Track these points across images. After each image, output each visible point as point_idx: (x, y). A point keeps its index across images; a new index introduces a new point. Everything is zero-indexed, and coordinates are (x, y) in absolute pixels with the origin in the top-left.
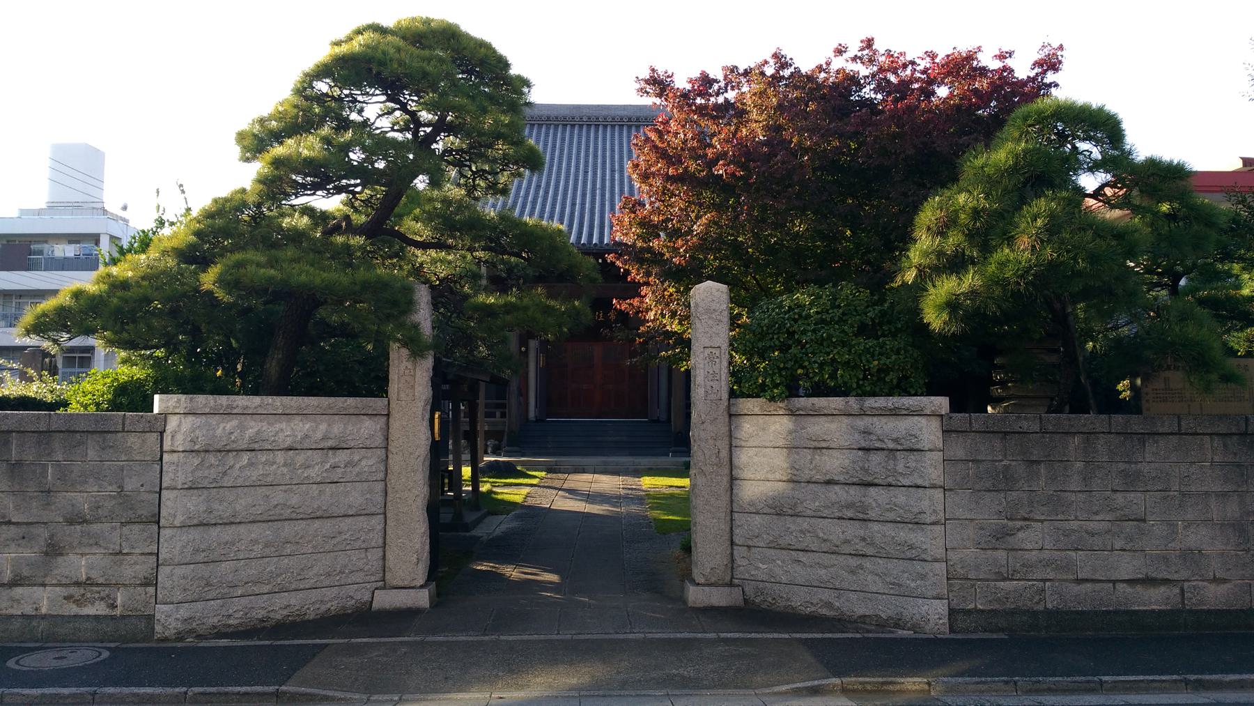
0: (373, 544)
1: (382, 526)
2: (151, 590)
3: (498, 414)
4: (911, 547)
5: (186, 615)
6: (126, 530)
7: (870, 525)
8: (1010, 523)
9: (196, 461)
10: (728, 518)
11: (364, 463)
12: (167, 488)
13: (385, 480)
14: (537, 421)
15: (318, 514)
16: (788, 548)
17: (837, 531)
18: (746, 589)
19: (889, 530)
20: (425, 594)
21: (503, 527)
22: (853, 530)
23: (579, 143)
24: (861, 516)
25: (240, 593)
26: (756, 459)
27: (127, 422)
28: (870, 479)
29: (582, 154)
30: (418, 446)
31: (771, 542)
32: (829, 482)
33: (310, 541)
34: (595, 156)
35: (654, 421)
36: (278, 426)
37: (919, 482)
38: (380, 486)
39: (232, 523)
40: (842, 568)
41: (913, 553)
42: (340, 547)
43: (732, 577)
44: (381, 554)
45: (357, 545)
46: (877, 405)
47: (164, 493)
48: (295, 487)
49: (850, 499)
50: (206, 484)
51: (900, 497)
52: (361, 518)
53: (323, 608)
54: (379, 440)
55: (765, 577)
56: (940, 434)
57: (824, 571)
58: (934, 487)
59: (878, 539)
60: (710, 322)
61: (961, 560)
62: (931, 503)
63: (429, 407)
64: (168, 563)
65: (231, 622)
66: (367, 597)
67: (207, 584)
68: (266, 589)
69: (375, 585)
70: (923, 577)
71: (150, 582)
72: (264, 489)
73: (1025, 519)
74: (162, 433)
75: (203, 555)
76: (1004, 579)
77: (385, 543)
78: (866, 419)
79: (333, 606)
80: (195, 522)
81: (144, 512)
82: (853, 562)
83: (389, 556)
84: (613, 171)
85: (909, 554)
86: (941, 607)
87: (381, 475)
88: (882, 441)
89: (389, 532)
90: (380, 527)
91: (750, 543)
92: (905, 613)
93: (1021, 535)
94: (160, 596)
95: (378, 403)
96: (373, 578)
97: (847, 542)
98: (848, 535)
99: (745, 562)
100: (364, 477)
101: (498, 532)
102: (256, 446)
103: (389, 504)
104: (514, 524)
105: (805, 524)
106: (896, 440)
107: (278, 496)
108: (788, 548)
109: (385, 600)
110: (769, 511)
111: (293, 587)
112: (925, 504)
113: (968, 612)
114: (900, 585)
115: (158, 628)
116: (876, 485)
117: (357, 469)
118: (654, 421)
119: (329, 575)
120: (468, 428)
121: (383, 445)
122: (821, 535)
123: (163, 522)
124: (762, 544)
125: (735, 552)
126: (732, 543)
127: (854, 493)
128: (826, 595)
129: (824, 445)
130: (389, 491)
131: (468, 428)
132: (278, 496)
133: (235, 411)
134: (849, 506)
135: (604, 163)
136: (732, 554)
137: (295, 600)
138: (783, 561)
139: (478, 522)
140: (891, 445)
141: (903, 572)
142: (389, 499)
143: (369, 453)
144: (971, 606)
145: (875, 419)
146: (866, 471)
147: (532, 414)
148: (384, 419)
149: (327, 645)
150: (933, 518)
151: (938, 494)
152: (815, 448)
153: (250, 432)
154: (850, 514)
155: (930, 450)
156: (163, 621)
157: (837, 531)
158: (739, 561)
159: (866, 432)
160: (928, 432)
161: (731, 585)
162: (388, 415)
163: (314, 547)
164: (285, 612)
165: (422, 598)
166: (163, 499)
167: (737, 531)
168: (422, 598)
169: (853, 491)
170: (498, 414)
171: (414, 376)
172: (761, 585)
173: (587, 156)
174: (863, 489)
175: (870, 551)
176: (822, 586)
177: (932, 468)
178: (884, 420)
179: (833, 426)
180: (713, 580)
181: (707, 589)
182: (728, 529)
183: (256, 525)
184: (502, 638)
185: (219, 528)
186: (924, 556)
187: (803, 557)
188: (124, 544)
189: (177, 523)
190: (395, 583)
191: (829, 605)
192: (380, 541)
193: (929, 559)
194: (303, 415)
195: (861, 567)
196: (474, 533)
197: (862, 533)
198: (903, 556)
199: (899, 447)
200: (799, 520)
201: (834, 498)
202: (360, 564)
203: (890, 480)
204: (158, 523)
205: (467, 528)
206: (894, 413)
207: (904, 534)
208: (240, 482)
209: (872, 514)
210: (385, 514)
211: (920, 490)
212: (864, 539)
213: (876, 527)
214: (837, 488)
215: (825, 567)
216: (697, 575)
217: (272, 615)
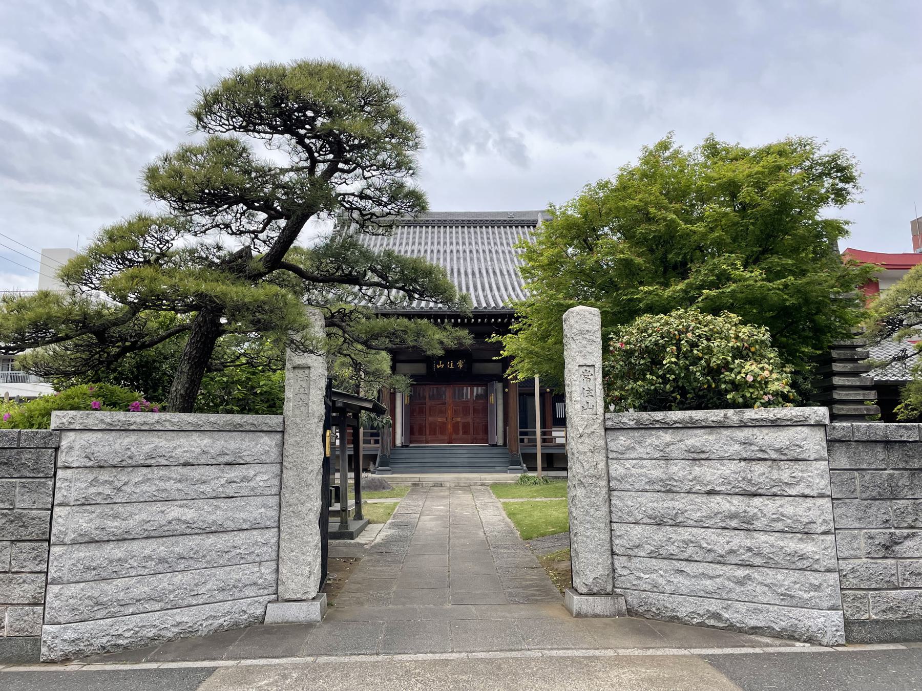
0: (267, 558)
1: (276, 539)
2: (39, 609)
3: (372, 442)
4: (802, 557)
5: (74, 636)
6: (15, 549)
7: (755, 534)
8: (897, 531)
9: (91, 477)
10: (608, 529)
11: (258, 478)
12: (60, 505)
13: (279, 494)
14: (402, 446)
15: (213, 528)
16: (670, 557)
17: (720, 541)
18: (629, 599)
19: (771, 538)
20: (317, 605)
21: (383, 534)
22: (739, 540)
23: (432, 239)
24: (746, 526)
25: (131, 611)
26: (634, 471)
27: (23, 438)
28: (754, 489)
29: (435, 246)
30: (312, 462)
31: (652, 552)
32: (710, 493)
33: (204, 556)
34: (445, 248)
35: (493, 446)
36: (176, 443)
37: (807, 492)
38: (273, 501)
39: (125, 539)
40: (729, 579)
41: (806, 563)
42: (234, 561)
43: (614, 587)
44: (275, 567)
45: (250, 559)
46: (756, 417)
47: (56, 509)
48: (191, 503)
49: (733, 509)
50: (99, 500)
51: (789, 508)
52: (255, 532)
53: (217, 623)
54: (274, 454)
55: (648, 587)
56: (824, 444)
57: (708, 582)
58: (822, 496)
59: (766, 550)
60: (584, 342)
61: (853, 570)
62: (819, 512)
63: (322, 424)
64: (55, 582)
65: (121, 642)
66: (259, 611)
67: (97, 604)
68: (157, 606)
69: (267, 598)
70: (817, 588)
71: (38, 602)
72: (159, 504)
73: (911, 527)
74: (57, 449)
75: (94, 573)
76: (896, 589)
77: (278, 556)
78: (746, 430)
79: (224, 621)
80: (87, 539)
81: (34, 531)
82: (741, 573)
83: (283, 570)
84: (458, 258)
85: (799, 565)
86: (837, 617)
87: (275, 490)
88: (764, 451)
89: (282, 544)
90: (274, 540)
91: (631, 553)
92: (800, 625)
93: (908, 543)
94: (47, 616)
95: (273, 420)
96: (266, 592)
97: (732, 552)
98: (734, 545)
99: (626, 572)
100: (259, 491)
101: (378, 540)
102: (153, 462)
103: (283, 518)
104: (391, 532)
105: (686, 533)
106: (777, 450)
107: (174, 512)
108: (670, 557)
109: (277, 613)
110: (649, 521)
111: (186, 602)
112: (813, 514)
113: (862, 623)
114: (792, 597)
115: (44, 650)
116: (761, 495)
117: (252, 484)
118: (493, 446)
119: (222, 590)
120: (352, 453)
121: (278, 460)
122: (705, 545)
123: (53, 539)
124: (643, 554)
125: (616, 563)
126: (613, 553)
127: (737, 504)
128: (714, 606)
129: (703, 456)
130: (283, 505)
131: (352, 453)
132: (174, 512)
133: (132, 427)
134: (733, 516)
135: (451, 252)
136: (612, 563)
137: (186, 617)
138: (666, 571)
139: (362, 529)
140: (774, 456)
141: (795, 583)
142: (283, 512)
143: (264, 468)
144: (866, 616)
145: (755, 430)
146: (750, 481)
147: (398, 442)
148: (280, 435)
149: (214, 669)
150: (823, 528)
151: (826, 503)
152: (694, 460)
153: (147, 448)
154: (734, 523)
155: (815, 460)
156: (49, 643)
157: (720, 541)
158: (619, 571)
159: (746, 443)
160: (813, 442)
161: (612, 594)
162: (283, 432)
163: (207, 562)
164: (176, 630)
165: (313, 611)
166: (55, 516)
167: (617, 542)
168: (313, 611)
169: (736, 500)
170: (372, 442)
171: (308, 394)
172: (644, 595)
173: (438, 248)
174: (746, 499)
175: (758, 561)
176: (708, 595)
177: (816, 476)
178: (765, 431)
179: (712, 438)
180: (595, 590)
181: (591, 598)
182: (608, 539)
183: (150, 541)
184: (397, 657)
185: (111, 545)
186: (816, 566)
187: (689, 568)
188: (13, 563)
189: (67, 540)
190: (287, 596)
191: (716, 616)
192: (274, 555)
193: (822, 569)
194: (198, 430)
195: (748, 578)
196: (360, 540)
197: (748, 543)
198: (793, 566)
199: (783, 457)
200: (681, 530)
201: (716, 508)
202: (254, 578)
203: (775, 490)
204: (49, 541)
205: (351, 536)
206: (776, 424)
207: (792, 544)
208: (134, 498)
209: (757, 524)
210: (279, 527)
211: (808, 500)
212: (750, 550)
213: (763, 537)
214: (718, 498)
215: (711, 578)
216: (578, 582)
217: (163, 633)
